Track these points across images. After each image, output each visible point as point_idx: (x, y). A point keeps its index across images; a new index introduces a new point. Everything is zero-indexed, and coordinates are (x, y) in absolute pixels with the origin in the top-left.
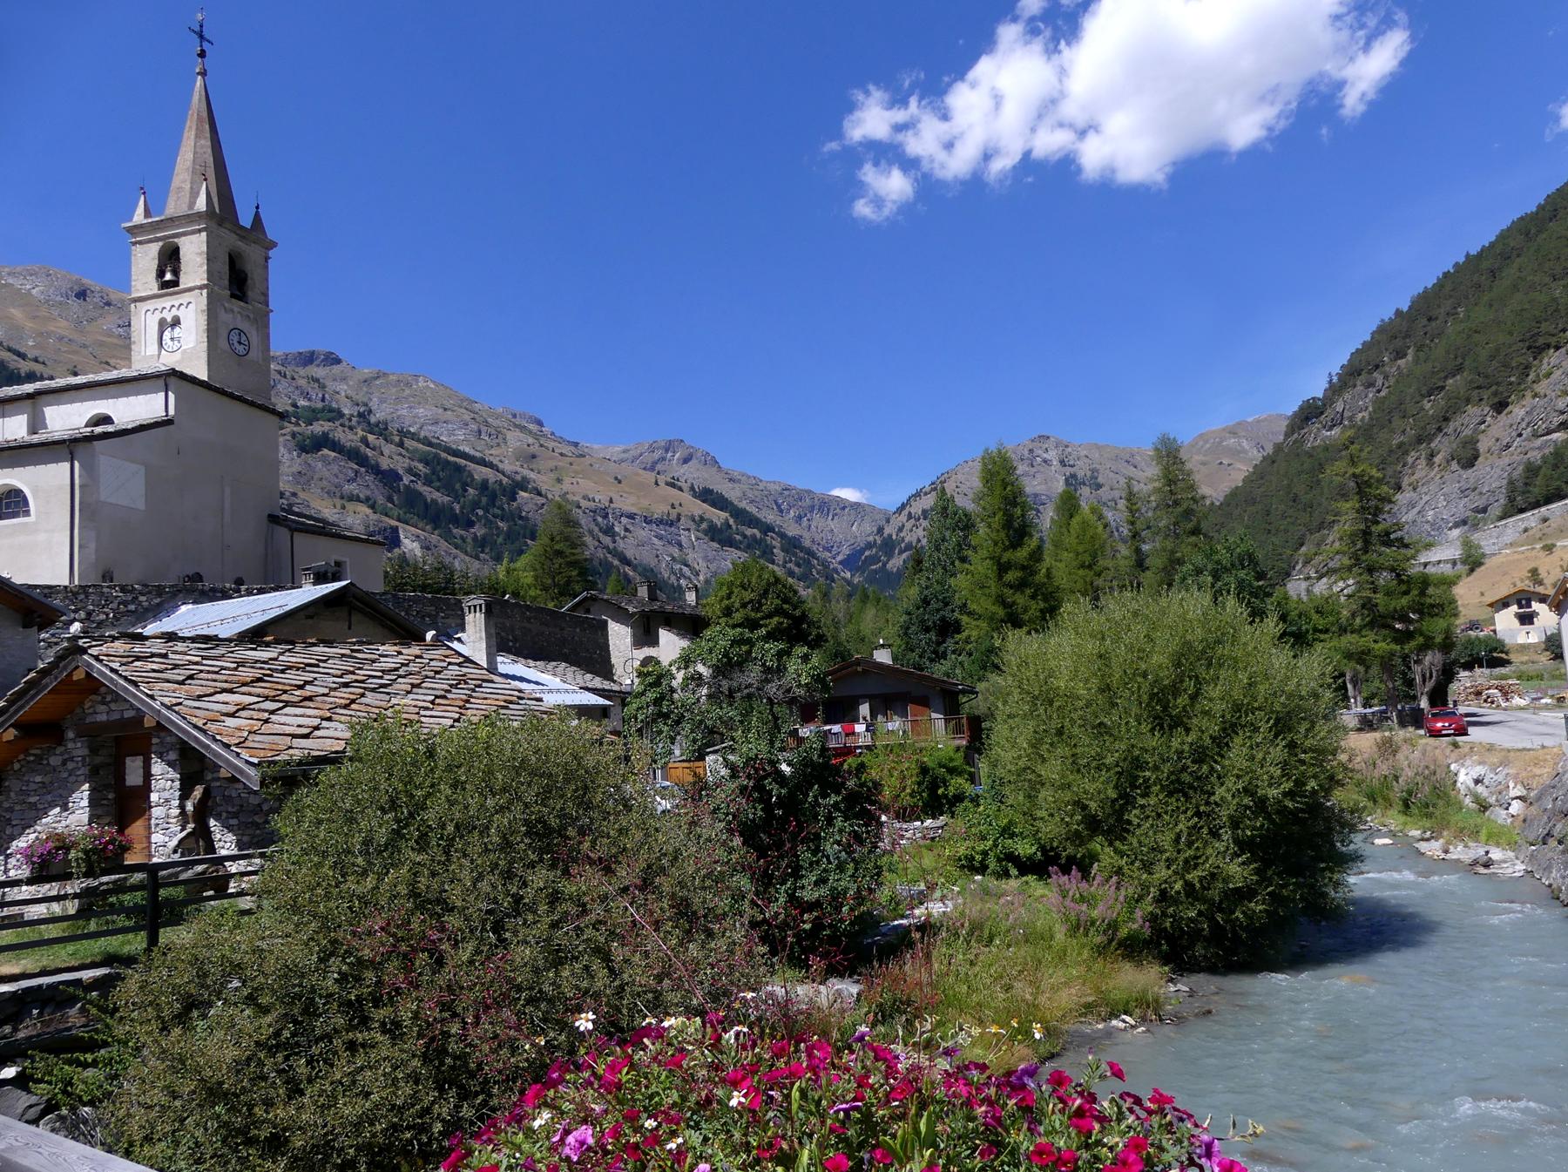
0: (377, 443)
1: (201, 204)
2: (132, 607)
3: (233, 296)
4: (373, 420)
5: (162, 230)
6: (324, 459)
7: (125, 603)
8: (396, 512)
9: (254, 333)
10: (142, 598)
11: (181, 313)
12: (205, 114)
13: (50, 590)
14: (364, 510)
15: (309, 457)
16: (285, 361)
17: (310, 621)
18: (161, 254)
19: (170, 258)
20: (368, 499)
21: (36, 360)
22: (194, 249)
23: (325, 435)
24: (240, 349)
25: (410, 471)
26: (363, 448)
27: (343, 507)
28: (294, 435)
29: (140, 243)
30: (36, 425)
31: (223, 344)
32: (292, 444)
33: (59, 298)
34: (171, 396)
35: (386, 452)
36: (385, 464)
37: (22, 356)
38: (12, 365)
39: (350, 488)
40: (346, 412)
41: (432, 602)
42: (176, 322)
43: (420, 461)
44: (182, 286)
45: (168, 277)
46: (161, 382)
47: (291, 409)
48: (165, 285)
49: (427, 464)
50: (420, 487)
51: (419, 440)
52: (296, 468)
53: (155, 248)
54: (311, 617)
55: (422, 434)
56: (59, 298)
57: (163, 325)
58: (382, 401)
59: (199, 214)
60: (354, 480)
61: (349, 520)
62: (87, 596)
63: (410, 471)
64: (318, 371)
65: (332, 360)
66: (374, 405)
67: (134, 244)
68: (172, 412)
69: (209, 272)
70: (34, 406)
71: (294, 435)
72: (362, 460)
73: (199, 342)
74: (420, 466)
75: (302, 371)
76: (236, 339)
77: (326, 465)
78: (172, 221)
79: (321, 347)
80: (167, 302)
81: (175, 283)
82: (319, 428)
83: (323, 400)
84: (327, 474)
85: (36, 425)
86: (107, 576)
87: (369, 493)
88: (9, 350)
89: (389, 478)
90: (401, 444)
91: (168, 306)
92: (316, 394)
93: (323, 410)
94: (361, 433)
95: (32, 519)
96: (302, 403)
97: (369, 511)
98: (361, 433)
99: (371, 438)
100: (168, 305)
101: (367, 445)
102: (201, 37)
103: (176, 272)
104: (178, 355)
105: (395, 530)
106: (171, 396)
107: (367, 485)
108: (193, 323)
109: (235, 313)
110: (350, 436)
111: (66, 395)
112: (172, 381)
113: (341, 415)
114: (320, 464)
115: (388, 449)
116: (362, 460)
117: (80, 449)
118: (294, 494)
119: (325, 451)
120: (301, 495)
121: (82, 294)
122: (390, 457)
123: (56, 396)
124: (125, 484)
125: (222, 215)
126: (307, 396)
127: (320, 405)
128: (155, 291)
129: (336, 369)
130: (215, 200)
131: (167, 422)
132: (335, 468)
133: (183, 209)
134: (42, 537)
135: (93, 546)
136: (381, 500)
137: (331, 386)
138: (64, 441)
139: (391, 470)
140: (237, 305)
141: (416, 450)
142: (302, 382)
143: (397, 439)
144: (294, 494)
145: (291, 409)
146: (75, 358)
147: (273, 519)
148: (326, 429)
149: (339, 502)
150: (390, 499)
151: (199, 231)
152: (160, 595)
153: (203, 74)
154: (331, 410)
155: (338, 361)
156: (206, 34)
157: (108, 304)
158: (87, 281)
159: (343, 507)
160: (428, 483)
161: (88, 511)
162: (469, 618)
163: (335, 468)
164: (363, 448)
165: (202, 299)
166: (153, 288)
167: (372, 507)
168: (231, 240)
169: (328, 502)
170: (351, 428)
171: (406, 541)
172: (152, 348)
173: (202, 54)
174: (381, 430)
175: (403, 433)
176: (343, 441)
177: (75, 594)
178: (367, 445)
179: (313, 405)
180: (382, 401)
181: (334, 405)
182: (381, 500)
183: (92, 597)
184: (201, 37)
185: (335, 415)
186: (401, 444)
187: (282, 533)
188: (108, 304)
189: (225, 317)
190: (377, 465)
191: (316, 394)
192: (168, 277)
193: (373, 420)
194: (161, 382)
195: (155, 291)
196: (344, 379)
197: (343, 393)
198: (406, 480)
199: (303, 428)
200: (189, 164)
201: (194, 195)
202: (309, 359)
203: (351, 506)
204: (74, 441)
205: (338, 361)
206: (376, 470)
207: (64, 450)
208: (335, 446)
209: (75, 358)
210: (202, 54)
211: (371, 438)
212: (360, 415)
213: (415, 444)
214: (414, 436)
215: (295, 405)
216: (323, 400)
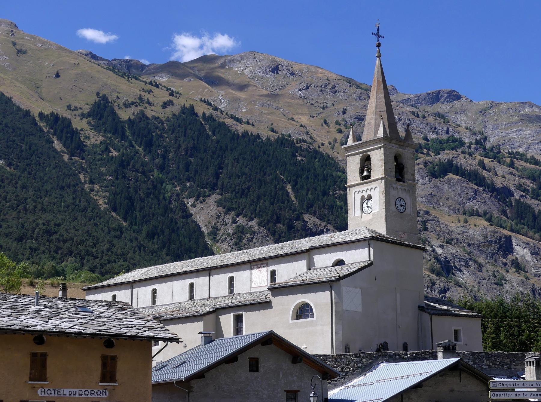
0: (492, 165)
1: (380, 134)
2: (360, 365)
3: (398, 180)
4: (488, 145)
5: (362, 148)
6: (450, 183)
7: (357, 363)
8: (509, 223)
9: (408, 198)
10: (364, 360)
11: (372, 193)
12: (381, 79)
13: (326, 357)
14: (483, 222)
15: (437, 181)
16: (417, 102)
17: (442, 378)
18: (362, 160)
19: (366, 162)
20: (485, 213)
21: (248, 123)
22: (377, 157)
23: (450, 162)
24: (401, 209)
25: (520, 187)
26: (480, 171)
27: (466, 221)
28: (426, 164)
29: (351, 155)
30: (310, 266)
31: (393, 208)
32: (424, 172)
33: (261, 74)
34: (372, 250)
35: (500, 172)
36: (499, 183)
37: (239, 120)
38: (233, 129)
39: (470, 205)
40: (466, 140)
41: (508, 356)
42: (370, 198)
43: (528, 178)
44: (372, 178)
45: (365, 173)
46: (367, 242)
47: (423, 142)
48: (364, 178)
49: (534, 180)
50: (529, 201)
51: (526, 160)
52: (428, 191)
53: (358, 158)
54: (442, 376)
55: (529, 156)
56: (261, 74)
57: (363, 198)
58: (495, 127)
59: (380, 139)
60: (474, 198)
61: (471, 232)
62: (341, 359)
63: (520, 187)
64: (442, 107)
65: (454, 96)
66: (488, 132)
67: (349, 156)
68: (372, 258)
69: (385, 170)
70: (309, 255)
71: (426, 164)
72: (479, 180)
73: (381, 209)
74: (528, 182)
75: (430, 109)
76: (399, 204)
77: (453, 187)
78: (367, 143)
79: (445, 87)
80: (365, 187)
81: (368, 177)
82: (445, 156)
83: (447, 132)
84: (452, 194)
85: (310, 266)
86: (347, 348)
87: (486, 208)
88: (232, 117)
89: (502, 194)
90: (512, 165)
91: (365, 189)
92: (442, 127)
93: (448, 140)
94: (478, 158)
95: (314, 319)
96: (431, 136)
97: (486, 224)
98: (478, 158)
99: (487, 161)
100: (365, 189)
101: (484, 168)
102: (378, 35)
103: (369, 171)
104: (370, 216)
105: (508, 239)
106: (372, 250)
107: (486, 202)
108: (378, 199)
109: (399, 190)
110: (470, 161)
111: (323, 249)
112: (372, 242)
113: (462, 144)
114: (446, 187)
115: (501, 170)
116: (479, 180)
117: (335, 285)
118: (427, 213)
119: (451, 175)
120: (433, 213)
121: (275, 70)
122: (503, 177)
123: (319, 250)
124: (353, 299)
125: (392, 138)
126: (435, 130)
127: (445, 137)
128: (359, 181)
129: (457, 104)
130: (387, 127)
131: (371, 264)
132: (458, 189)
133: (372, 138)
134: (319, 328)
135: (341, 332)
136: (496, 214)
137: (452, 117)
138: (328, 281)
139: (504, 187)
140: (399, 185)
141: (524, 169)
142: (431, 119)
143: (508, 160)
144: (427, 213)
145: (423, 142)
146: (271, 117)
147: (421, 308)
148: (451, 156)
149: (462, 218)
150: (504, 213)
151: (380, 148)
152: (371, 358)
153: (379, 56)
154: (454, 140)
155: (459, 97)
156: (381, 34)
157: (293, 74)
158: (278, 59)
159: (466, 221)
160: (536, 196)
161: (339, 315)
162: (527, 369)
163: (458, 189)
164: (480, 171)
165: (381, 186)
166: (358, 180)
167: (489, 220)
168: (395, 148)
169: (454, 218)
170: (470, 154)
171: (518, 249)
172: (358, 213)
173: (379, 45)
174: (495, 154)
175: (514, 155)
176: (464, 166)
177: (336, 359)
178: (484, 168)
179: (440, 137)
180: (495, 127)
181: (457, 136)
182: (496, 214)
183: (343, 360)
184: (378, 35)
185: (456, 144)
186: (512, 165)
187: (426, 316)
188: (293, 74)
189: (393, 192)
190: (493, 184)
191: (442, 127)
192: (365, 173)
193: (488, 145)
194: (367, 242)
195: (359, 181)
196: (463, 112)
197: (463, 123)
198: (517, 195)
199: (433, 158)
200: (374, 109)
201: (377, 127)
202: (435, 98)
203: (472, 220)
204: (333, 281)
205: (459, 97)
206: (492, 189)
207: (328, 285)
208: (458, 170)
209: (271, 117)
210: (379, 45)
211: (487, 161)
212: (478, 142)
213: (524, 163)
214: (522, 157)
215: (426, 139)
216: (447, 132)
